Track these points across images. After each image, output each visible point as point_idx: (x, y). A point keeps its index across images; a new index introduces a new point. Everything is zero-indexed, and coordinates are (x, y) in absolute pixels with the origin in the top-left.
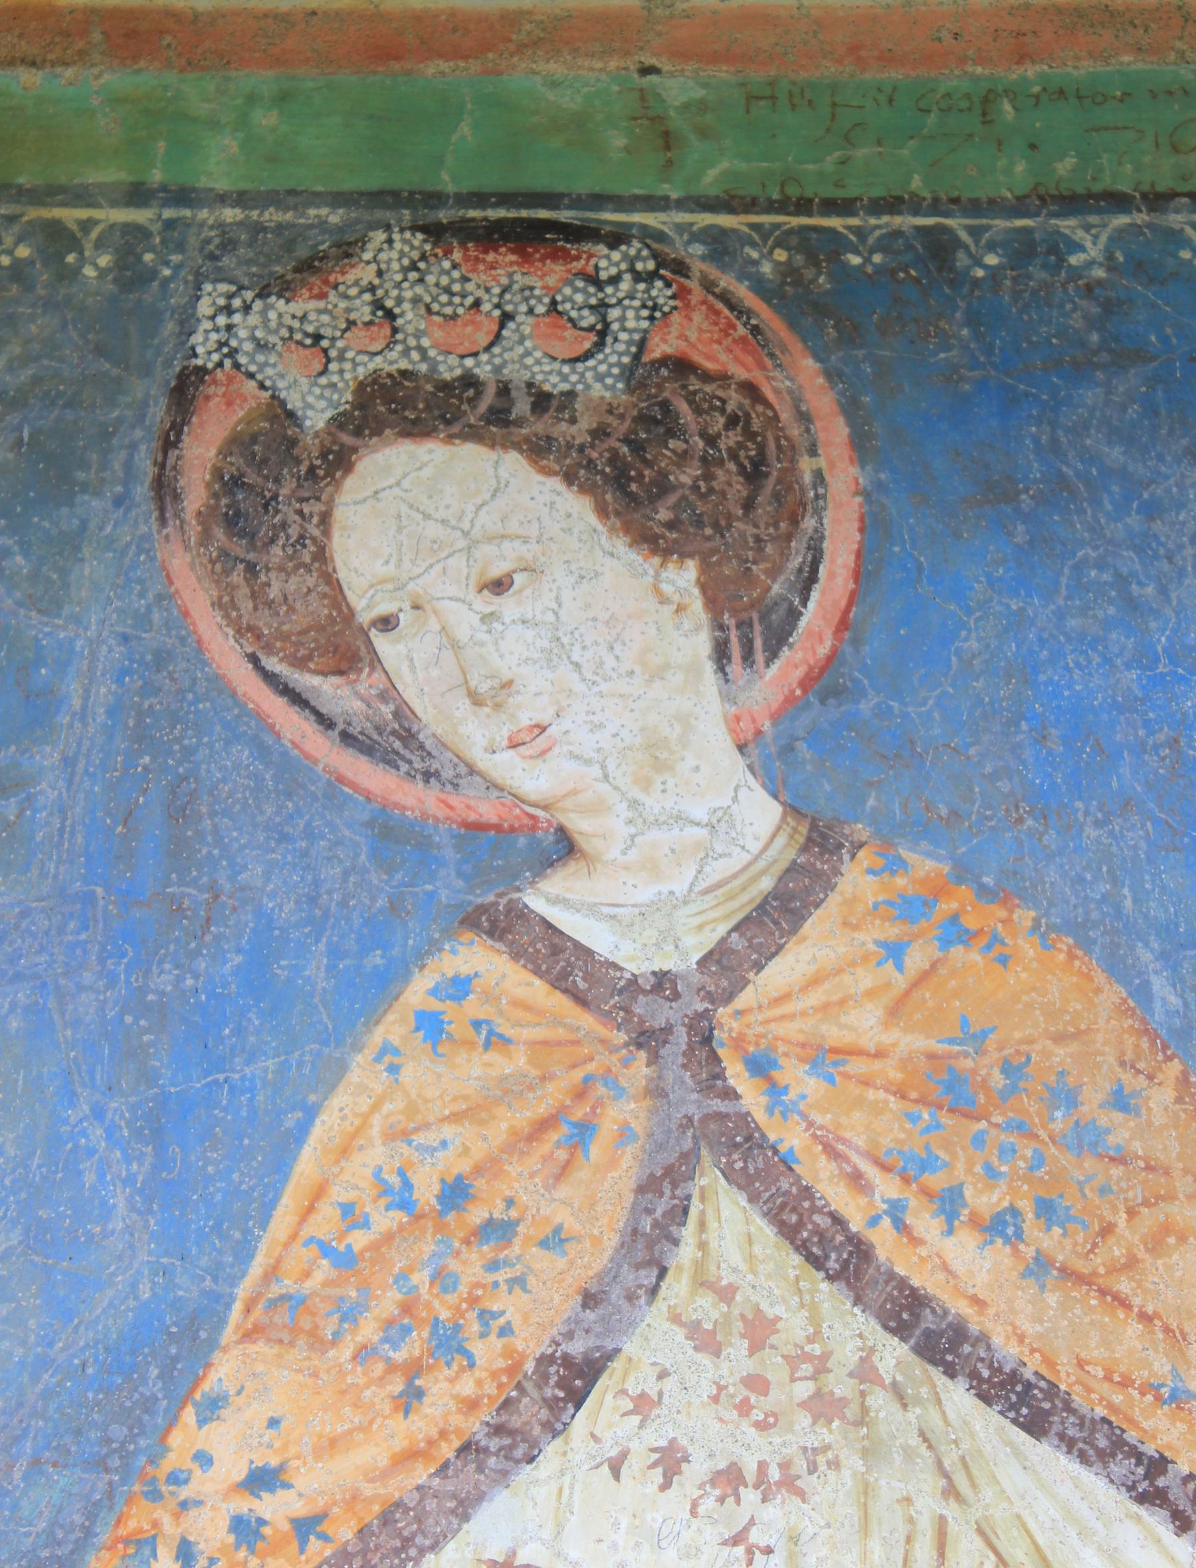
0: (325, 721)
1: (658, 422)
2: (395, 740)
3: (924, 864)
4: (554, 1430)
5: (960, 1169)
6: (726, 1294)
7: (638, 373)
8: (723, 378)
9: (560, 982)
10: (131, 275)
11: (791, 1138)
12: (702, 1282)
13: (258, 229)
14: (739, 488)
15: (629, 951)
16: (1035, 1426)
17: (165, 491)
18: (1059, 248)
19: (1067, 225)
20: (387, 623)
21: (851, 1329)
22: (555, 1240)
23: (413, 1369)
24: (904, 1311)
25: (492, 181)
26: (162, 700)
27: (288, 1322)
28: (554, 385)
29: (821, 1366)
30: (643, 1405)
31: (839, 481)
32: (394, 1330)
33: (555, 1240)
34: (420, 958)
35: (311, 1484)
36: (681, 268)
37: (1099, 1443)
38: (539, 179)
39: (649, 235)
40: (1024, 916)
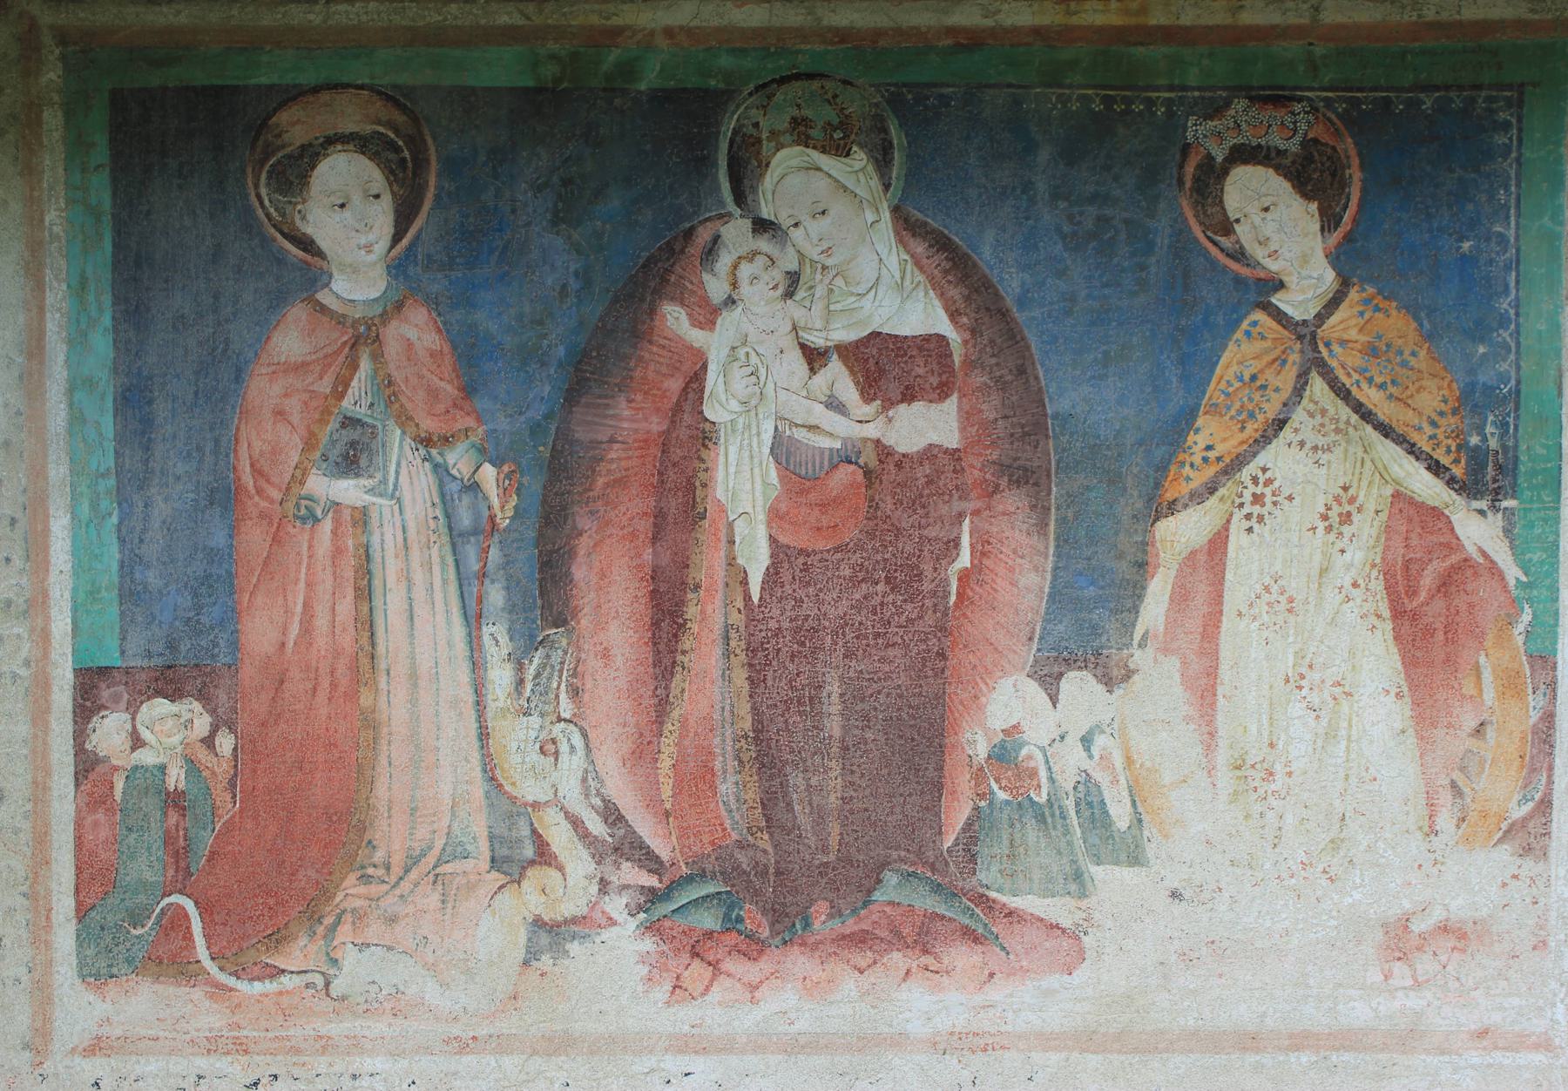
0: (1222, 250)
1: (1308, 159)
2: (1239, 255)
3: (1370, 290)
4: (1276, 436)
5: (1374, 372)
6: (1316, 403)
7: (1305, 143)
8: (1326, 145)
9: (1279, 322)
10: (1170, 114)
11: (1334, 364)
12: (1311, 400)
13: (1203, 98)
14: (1329, 179)
15: (1296, 314)
16: (1386, 436)
17: (1181, 182)
19: (1422, 95)
21: (1345, 412)
22: (1277, 390)
23: (1244, 422)
26: (1182, 245)
27: (1214, 409)
28: (1282, 147)
29: (1338, 421)
30: (1296, 431)
31: (1355, 175)
32: (1239, 412)
33: (1277, 390)
34: (1245, 316)
35: (1220, 449)
36: (1317, 110)
37: (1401, 440)
39: (1309, 99)
40: (1394, 304)
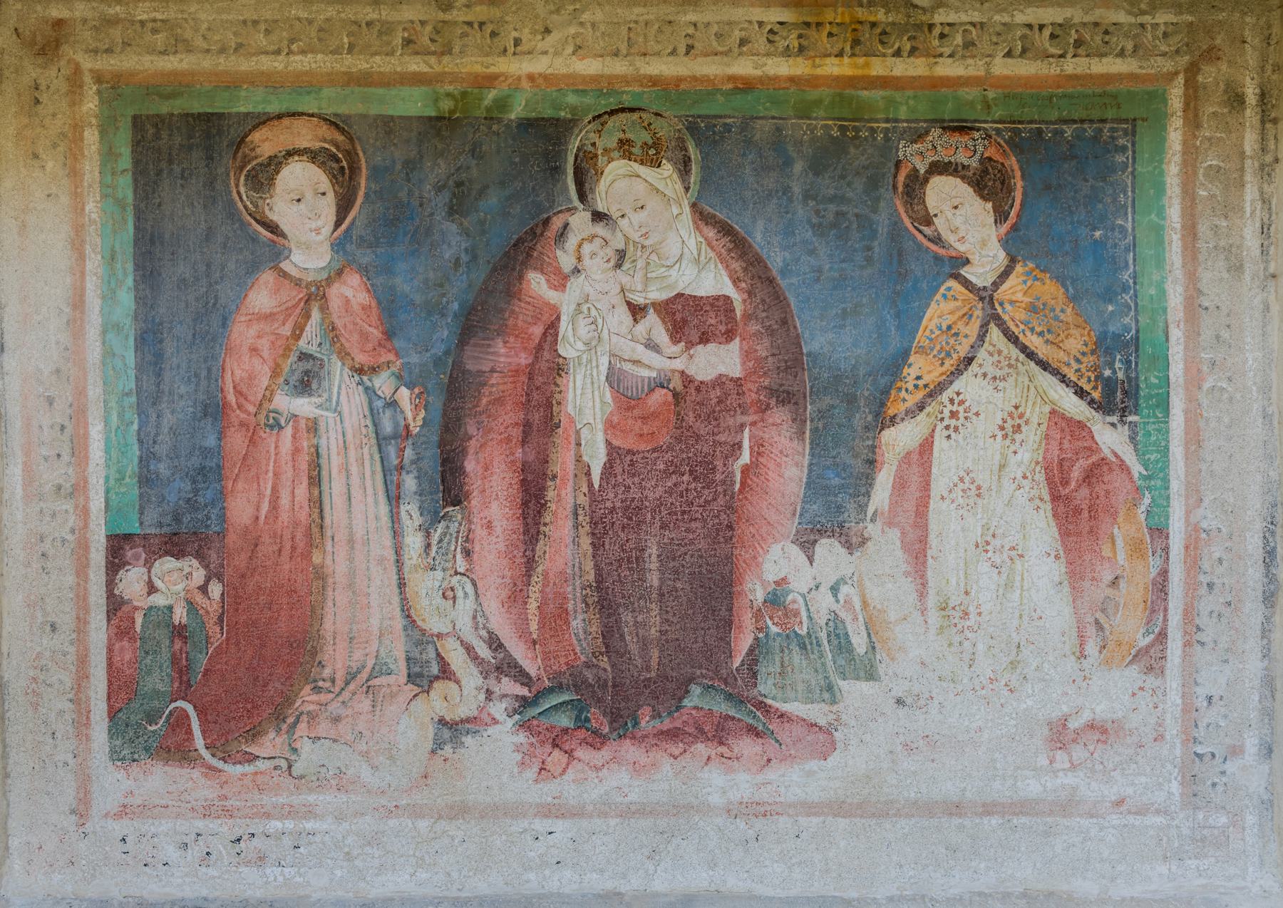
1: (985, 172)
2: (937, 240)
3: (1031, 265)
5: (1034, 323)
7: (982, 161)
9: (967, 288)
10: (887, 139)
11: (1006, 318)
15: (979, 282)
16: (1045, 369)
17: (895, 187)
18: (1062, 132)
20: (936, 215)
21: (1015, 352)
22: (966, 336)
24: (1024, 349)
25: (955, 117)
27: (922, 350)
30: (981, 365)
32: (940, 352)
33: (966, 336)
38: (964, 117)
39: (985, 129)
